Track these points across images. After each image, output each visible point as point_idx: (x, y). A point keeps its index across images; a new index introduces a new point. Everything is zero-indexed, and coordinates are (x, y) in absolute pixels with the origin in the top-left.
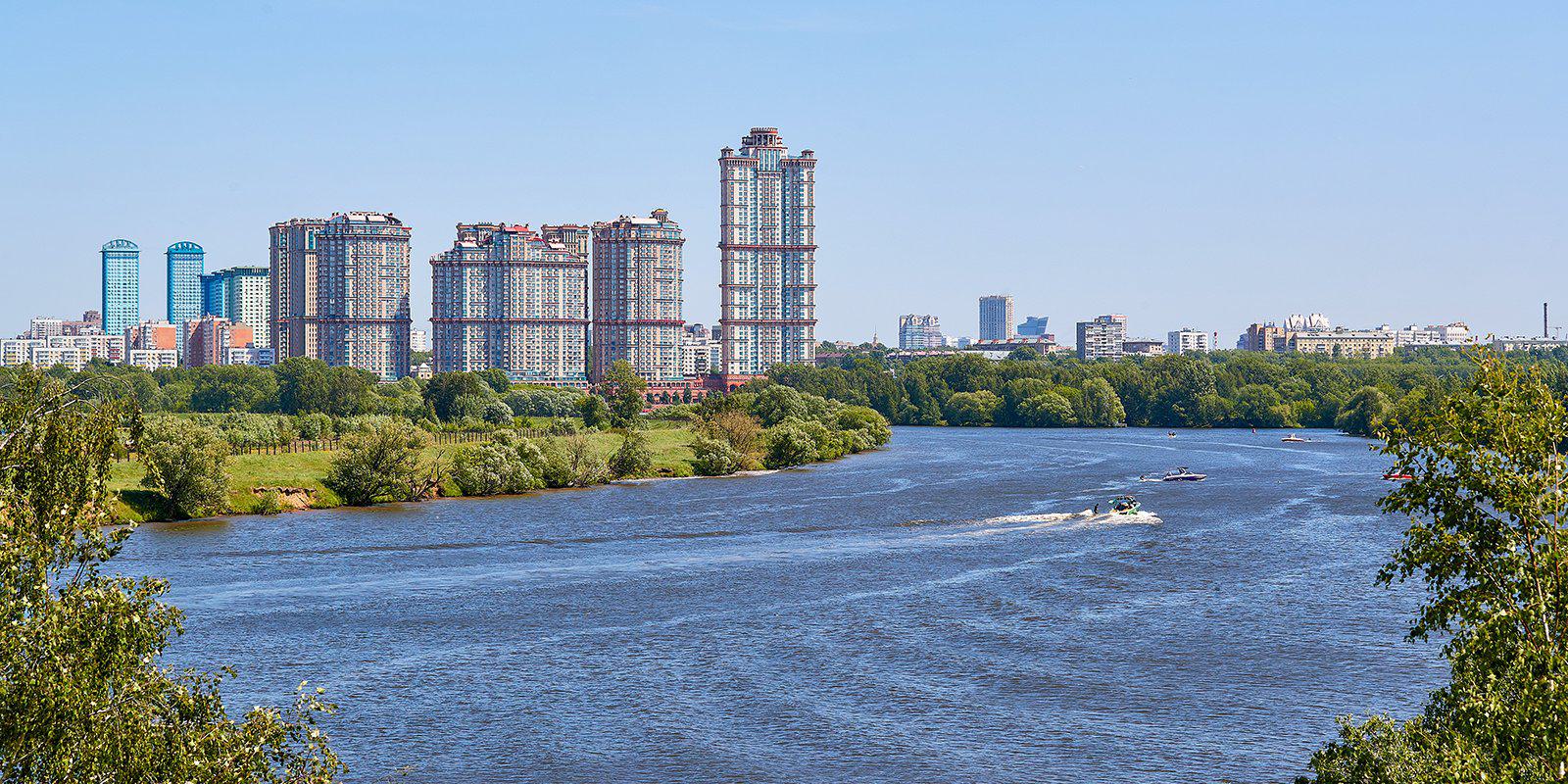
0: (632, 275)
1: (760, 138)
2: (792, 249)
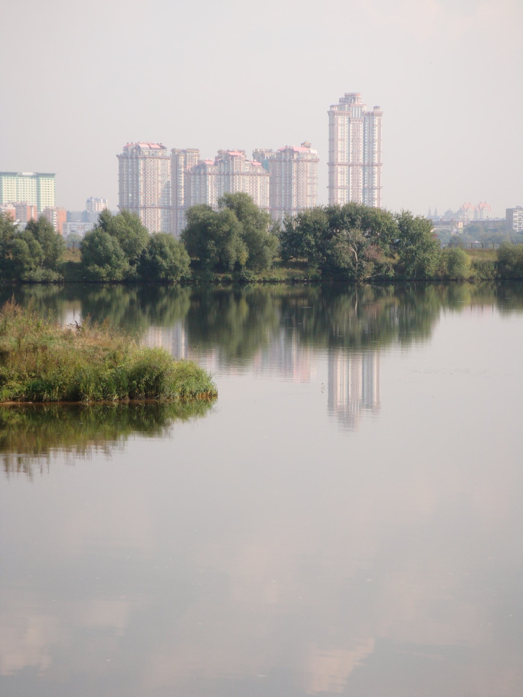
0: (294, 181)
1: (349, 99)
2: (368, 165)
